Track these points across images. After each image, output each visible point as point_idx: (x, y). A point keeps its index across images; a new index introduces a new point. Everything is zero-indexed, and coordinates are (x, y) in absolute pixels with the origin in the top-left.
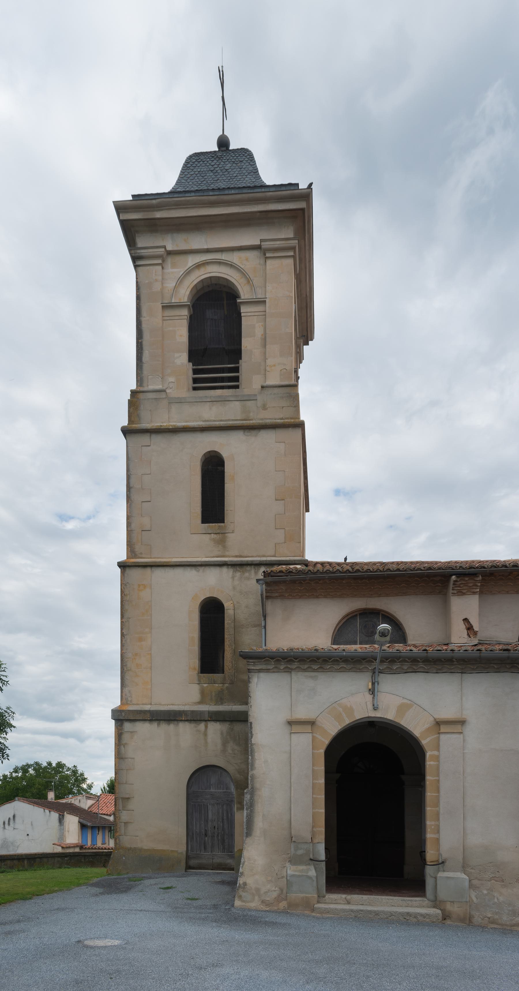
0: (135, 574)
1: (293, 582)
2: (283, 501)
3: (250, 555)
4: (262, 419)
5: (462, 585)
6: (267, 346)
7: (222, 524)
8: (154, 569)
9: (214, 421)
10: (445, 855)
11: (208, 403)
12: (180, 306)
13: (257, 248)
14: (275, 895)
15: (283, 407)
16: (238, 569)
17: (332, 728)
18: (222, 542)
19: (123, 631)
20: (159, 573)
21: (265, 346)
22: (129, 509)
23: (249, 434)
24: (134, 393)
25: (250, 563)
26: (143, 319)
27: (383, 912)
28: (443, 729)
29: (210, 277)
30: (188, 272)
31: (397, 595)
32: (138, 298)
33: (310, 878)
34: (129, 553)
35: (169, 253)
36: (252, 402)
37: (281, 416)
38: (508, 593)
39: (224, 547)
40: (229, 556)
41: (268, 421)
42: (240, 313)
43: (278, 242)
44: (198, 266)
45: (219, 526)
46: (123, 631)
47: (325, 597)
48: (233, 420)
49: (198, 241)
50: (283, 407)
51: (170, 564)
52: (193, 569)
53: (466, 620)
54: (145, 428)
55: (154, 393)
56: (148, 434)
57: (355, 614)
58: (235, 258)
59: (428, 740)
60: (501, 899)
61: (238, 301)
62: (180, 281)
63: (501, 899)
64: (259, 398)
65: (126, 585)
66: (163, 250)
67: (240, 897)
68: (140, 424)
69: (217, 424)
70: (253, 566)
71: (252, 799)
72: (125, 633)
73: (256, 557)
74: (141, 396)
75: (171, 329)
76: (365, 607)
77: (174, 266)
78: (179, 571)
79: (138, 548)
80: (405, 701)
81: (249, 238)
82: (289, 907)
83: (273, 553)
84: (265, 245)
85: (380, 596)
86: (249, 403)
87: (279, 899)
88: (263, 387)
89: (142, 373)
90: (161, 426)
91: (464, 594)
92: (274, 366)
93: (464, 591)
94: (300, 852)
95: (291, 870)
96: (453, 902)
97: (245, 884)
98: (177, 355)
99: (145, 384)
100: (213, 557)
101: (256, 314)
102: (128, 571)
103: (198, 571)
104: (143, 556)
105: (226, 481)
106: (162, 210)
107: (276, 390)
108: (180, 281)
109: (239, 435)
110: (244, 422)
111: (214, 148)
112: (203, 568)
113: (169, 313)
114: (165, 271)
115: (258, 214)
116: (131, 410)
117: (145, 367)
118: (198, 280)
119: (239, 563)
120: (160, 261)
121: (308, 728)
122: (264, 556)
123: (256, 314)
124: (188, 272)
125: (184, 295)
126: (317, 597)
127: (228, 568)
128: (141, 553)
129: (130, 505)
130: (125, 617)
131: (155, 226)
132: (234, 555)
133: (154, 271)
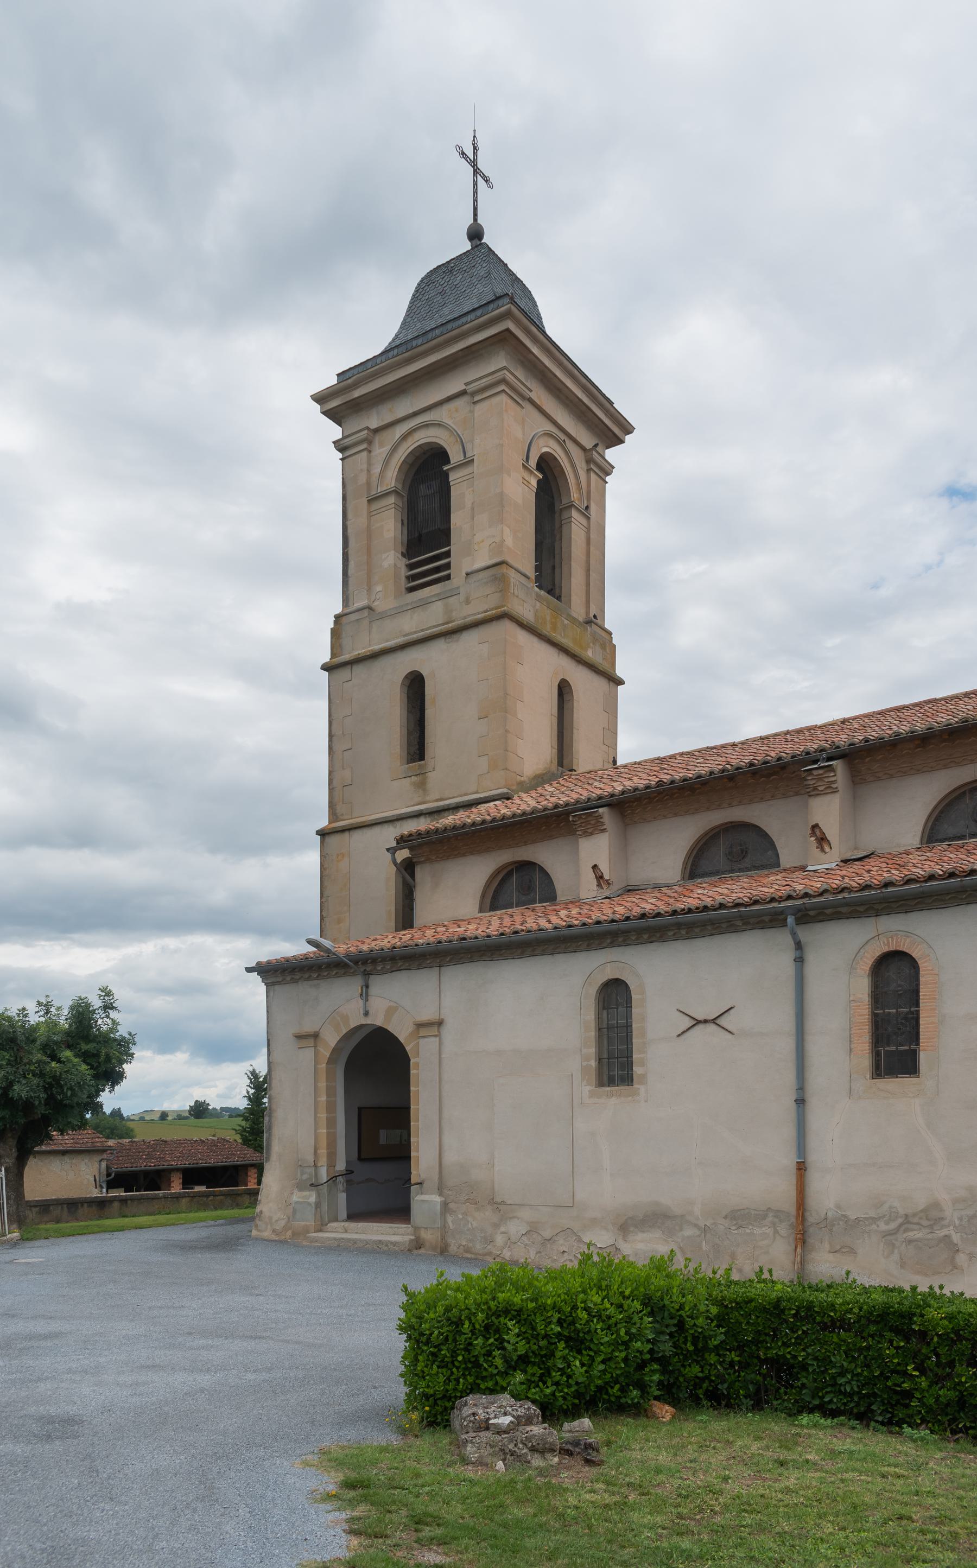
0: (333, 840)
1: (441, 841)
4: (465, 618)
8: (352, 832)
9: (415, 632)
10: (423, 1176)
12: (386, 495)
13: (463, 393)
14: (283, 1223)
17: (331, 1038)
18: (422, 785)
20: (357, 835)
24: (338, 618)
27: (360, 1240)
28: (423, 1032)
29: (419, 446)
30: (394, 449)
33: (309, 1204)
35: (376, 431)
38: (665, 817)
39: (425, 790)
40: (429, 802)
43: (484, 380)
44: (405, 437)
45: (420, 765)
47: (472, 853)
49: (403, 407)
52: (390, 824)
56: (349, 666)
57: (510, 868)
59: (411, 1045)
60: (475, 1224)
63: (475, 1224)
64: (462, 590)
66: (366, 432)
67: (256, 1226)
71: (270, 1121)
74: (344, 620)
77: (381, 445)
79: (340, 809)
80: (392, 1004)
81: (454, 384)
82: (290, 1240)
84: (471, 388)
85: (526, 844)
87: (286, 1228)
88: (467, 574)
91: (591, 834)
93: (590, 831)
94: (305, 1177)
95: (297, 1197)
96: (426, 1228)
97: (261, 1212)
99: (351, 603)
104: (345, 817)
105: (426, 707)
109: (440, 644)
113: (375, 506)
114: (373, 454)
118: (406, 454)
120: (364, 446)
121: (311, 1042)
122: (466, 794)
124: (394, 449)
125: (391, 479)
126: (464, 855)
128: (342, 815)
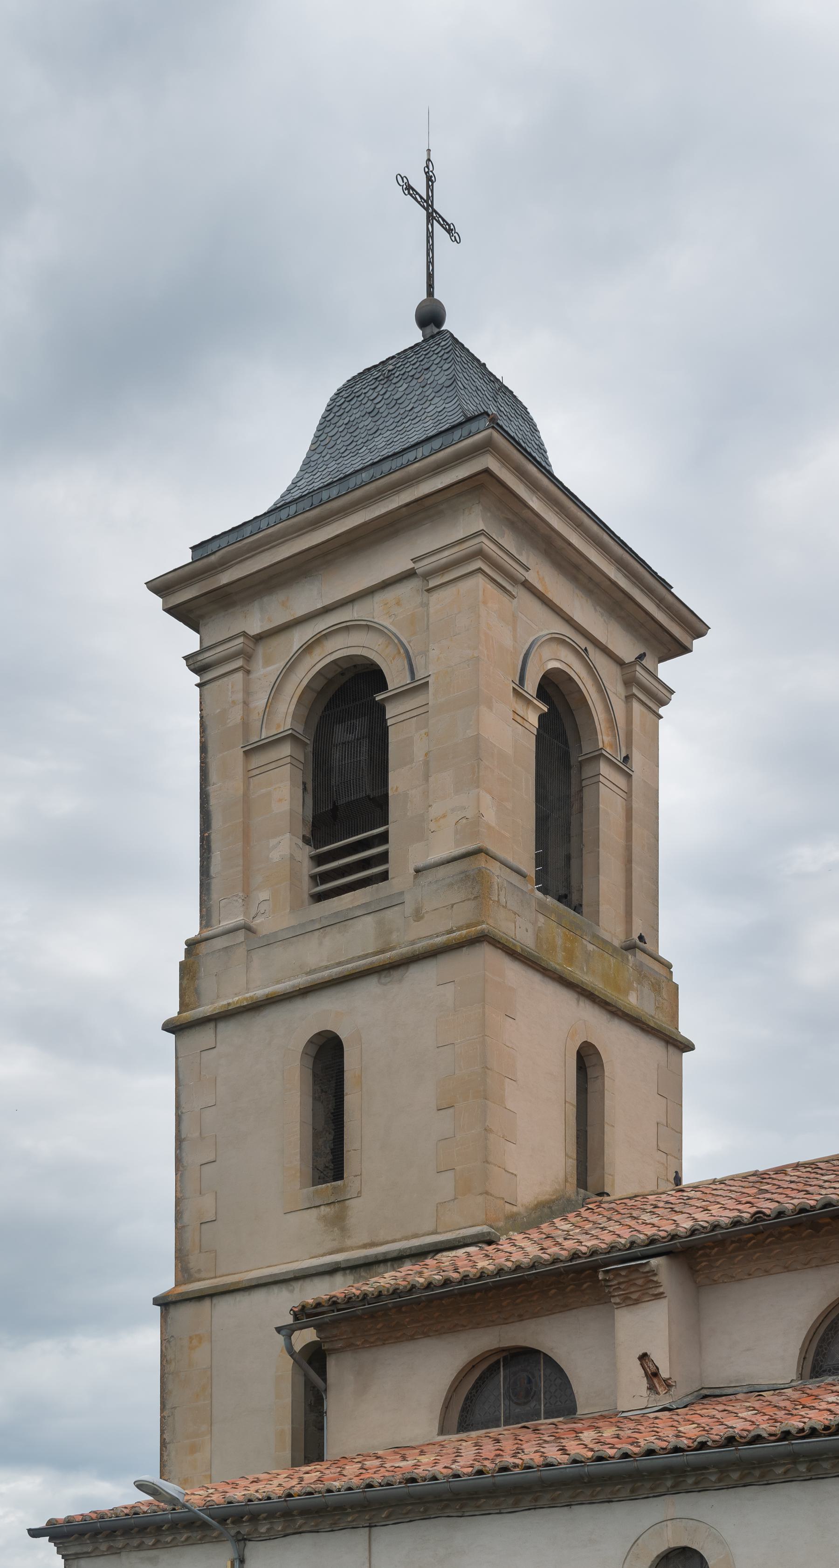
0: (183, 1314)
2: (451, 1110)
3: (390, 1239)
4: (413, 943)
5: (622, 1286)
6: (431, 779)
7: (339, 1183)
8: (216, 1300)
9: (327, 968)
11: (317, 933)
13: (409, 575)
15: (453, 905)
16: (363, 1274)
18: (338, 1221)
19: (165, 1436)
20: (224, 1305)
21: (427, 778)
22: (179, 1184)
23: (388, 979)
24: (192, 945)
25: (381, 1258)
26: (211, 789)
29: (334, 662)
30: (290, 667)
31: (551, 1312)
32: (204, 749)
34: (180, 1273)
36: (396, 908)
37: (442, 929)
38: (767, 1273)
39: (343, 1230)
40: (352, 1248)
41: (420, 946)
42: (385, 721)
43: (446, 553)
45: (334, 1188)
46: (165, 1436)
47: (426, 1335)
48: (360, 958)
49: (305, 598)
50: (453, 905)
51: (241, 1286)
53: (644, 1357)
54: (201, 1016)
55: (224, 937)
56: (212, 1025)
58: (372, 610)
61: (377, 699)
62: (277, 689)
64: (407, 898)
65: (169, 1342)
68: (199, 1006)
69: (335, 972)
70: (389, 1264)
72: (167, 1440)
73: (400, 1240)
75: (263, 791)
76: (497, 1346)
77: (268, 662)
78: (259, 1296)
79: (195, 1261)
81: (394, 560)
83: (429, 1226)
84: (422, 567)
85: (521, 1318)
86: (389, 913)
89: (209, 899)
90: (229, 1004)
91: (637, 1302)
92: (444, 816)
93: (634, 1296)
98: (273, 842)
99: (214, 921)
100: (324, 1255)
101: (414, 713)
102: (174, 1312)
103: (292, 1291)
106: (231, 566)
107: (442, 872)
108: (277, 691)
109: (371, 987)
110: (382, 956)
111: (416, 336)
112: (300, 1283)
113: (258, 760)
114: (253, 676)
115: (404, 509)
116: (185, 982)
117: (216, 884)
119: (361, 1262)
122: (416, 1236)
123: (414, 713)
124: (290, 667)
125: (285, 715)
126: (412, 1338)
127: (345, 1275)
128: (199, 1271)
129: (182, 1175)
130: (167, 1407)
131: (226, 599)
132: (361, 1243)
133: (230, 686)
